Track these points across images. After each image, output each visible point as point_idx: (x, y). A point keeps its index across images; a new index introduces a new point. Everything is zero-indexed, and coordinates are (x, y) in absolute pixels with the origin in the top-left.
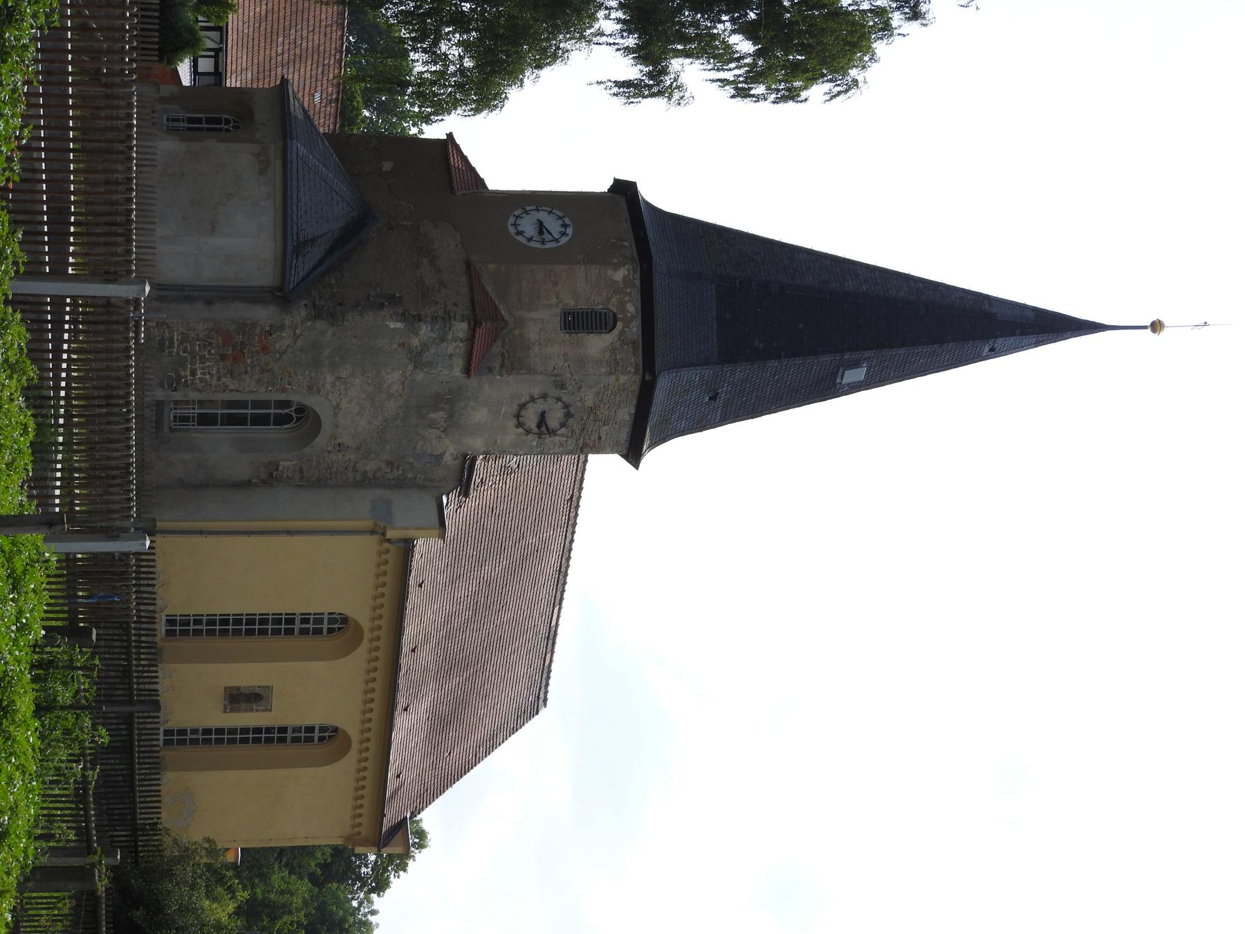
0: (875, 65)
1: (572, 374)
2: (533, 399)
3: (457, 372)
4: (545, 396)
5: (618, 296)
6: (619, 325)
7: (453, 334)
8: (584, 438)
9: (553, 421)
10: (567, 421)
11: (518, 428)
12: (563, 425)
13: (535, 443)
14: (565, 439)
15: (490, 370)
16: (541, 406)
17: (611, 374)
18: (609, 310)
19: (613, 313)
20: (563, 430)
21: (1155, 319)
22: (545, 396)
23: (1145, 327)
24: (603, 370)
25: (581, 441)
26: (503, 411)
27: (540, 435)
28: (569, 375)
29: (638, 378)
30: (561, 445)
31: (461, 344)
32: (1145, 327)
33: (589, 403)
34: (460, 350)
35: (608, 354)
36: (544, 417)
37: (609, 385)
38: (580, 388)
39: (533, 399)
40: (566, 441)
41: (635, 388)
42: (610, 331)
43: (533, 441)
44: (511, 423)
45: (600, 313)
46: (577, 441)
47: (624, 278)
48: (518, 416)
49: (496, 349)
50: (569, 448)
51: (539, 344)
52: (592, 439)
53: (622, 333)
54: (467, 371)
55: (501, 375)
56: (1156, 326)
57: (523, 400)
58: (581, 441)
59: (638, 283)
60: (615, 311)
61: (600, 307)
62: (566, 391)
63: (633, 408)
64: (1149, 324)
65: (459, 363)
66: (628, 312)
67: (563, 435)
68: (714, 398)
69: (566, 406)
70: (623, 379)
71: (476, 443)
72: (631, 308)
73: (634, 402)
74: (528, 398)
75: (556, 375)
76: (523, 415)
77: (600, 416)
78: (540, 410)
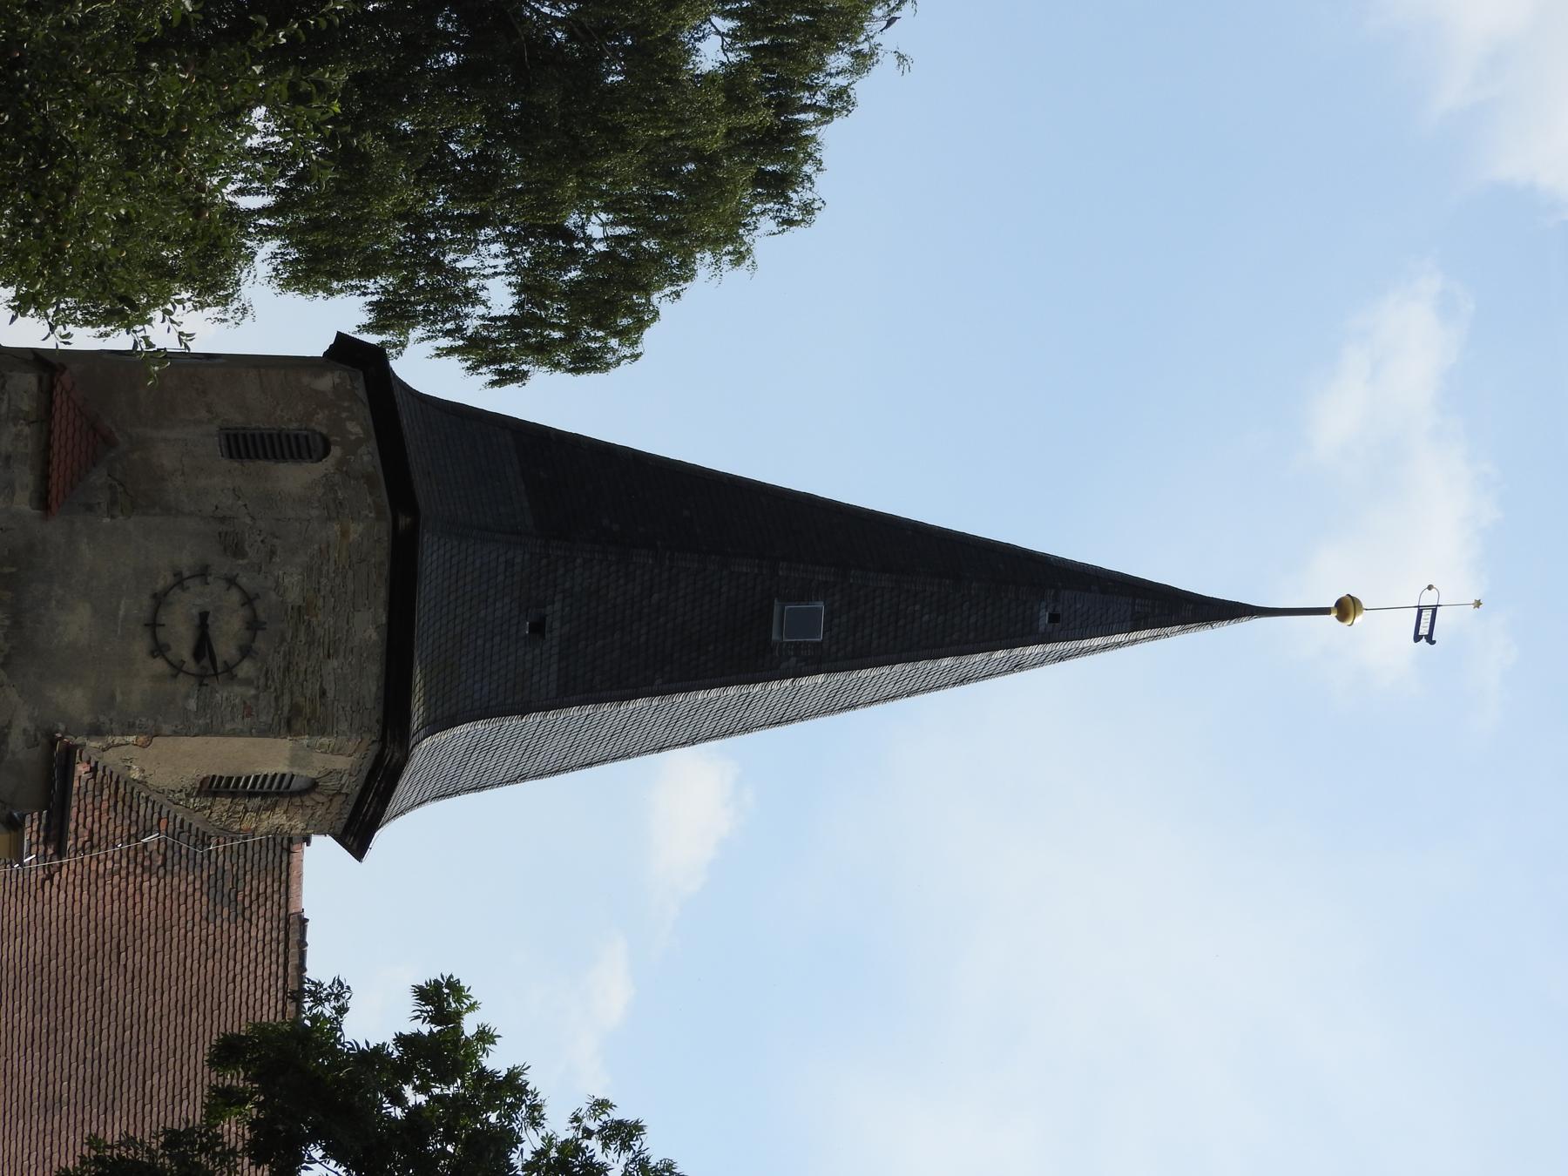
0: (855, 108)
1: (253, 518)
2: (180, 581)
3: (23, 503)
4: (203, 573)
5: (326, 412)
6: (336, 451)
7: (9, 400)
8: (292, 693)
9: (227, 636)
10: (253, 640)
11: (155, 657)
12: (246, 651)
13: (192, 704)
14: (253, 692)
15: (89, 508)
16: (198, 601)
17: (329, 519)
18: (314, 431)
19: (321, 434)
20: (246, 669)
21: (1344, 595)
22: (203, 573)
23: (1324, 611)
24: (314, 513)
25: (286, 699)
26: (121, 613)
27: (201, 679)
28: (248, 520)
29: (383, 530)
30: (248, 711)
31: (27, 430)
32: (1324, 611)
33: (294, 597)
34: (26, 446)
35: (320, 491)
36: (207, 626)
37: (328, 546)
38: (273, 553)
39: (180, 581)
40: (256, 697)
41: (381, 554)
42: (320, 460)
43: (187, 697)
44: (140, 646)
45: (297, 437)
46: (277, 699)
47: (335, 387)
48: (153, 625)
49: (98, 477)
50: (263, 718)
51: (183, 474)
52: (308, 696)
53: (341, 462)
54: (44, 502)
55: (113, 517)
56: (1346, 608)
57: (161, 585)
58: (286, 699)
59: (361, 393)
60: (325, 431)
61: (294, 425)
62: (246, 561)
63: (381, 610)
64: (1332, 605)
65: (25, 478)
66: (351, 433)
67: (248, 682)
68: (538, 628)
69: (249, 600)
70: (356, 530)
71: (73, 700)
72: (354, 429)
73: (383, 594)
74: (170, 579)
75: (223, 520)
76: (162, 623)
77: (320, 632)
78: (195, 611)
